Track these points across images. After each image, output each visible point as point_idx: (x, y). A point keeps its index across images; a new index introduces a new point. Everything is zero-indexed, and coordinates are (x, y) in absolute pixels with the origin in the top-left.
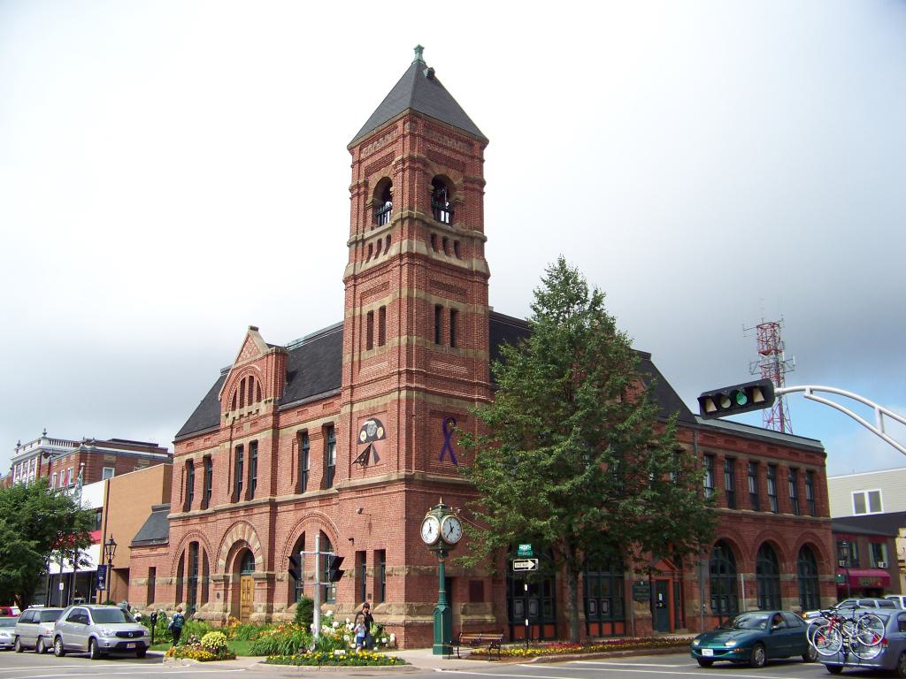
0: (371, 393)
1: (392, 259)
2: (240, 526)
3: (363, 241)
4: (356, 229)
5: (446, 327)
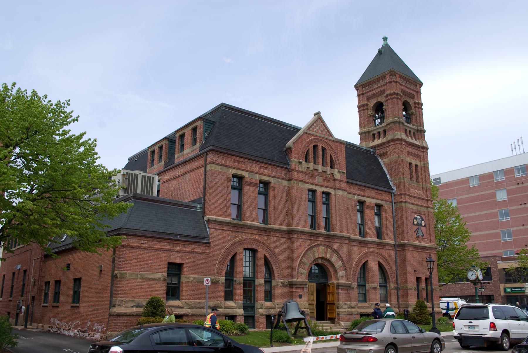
1: (389, 142)
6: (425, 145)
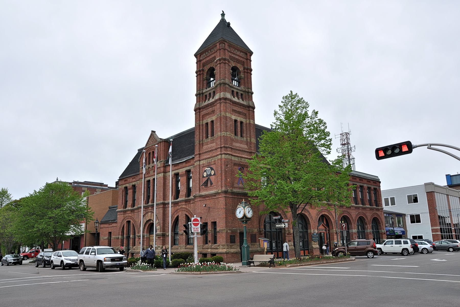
0: (208, 156)
1: (216, 101)
2: (150, 213)
3: (203, 93)
4: (198, 89)
5: (239, 128)
6: (251, 105)
